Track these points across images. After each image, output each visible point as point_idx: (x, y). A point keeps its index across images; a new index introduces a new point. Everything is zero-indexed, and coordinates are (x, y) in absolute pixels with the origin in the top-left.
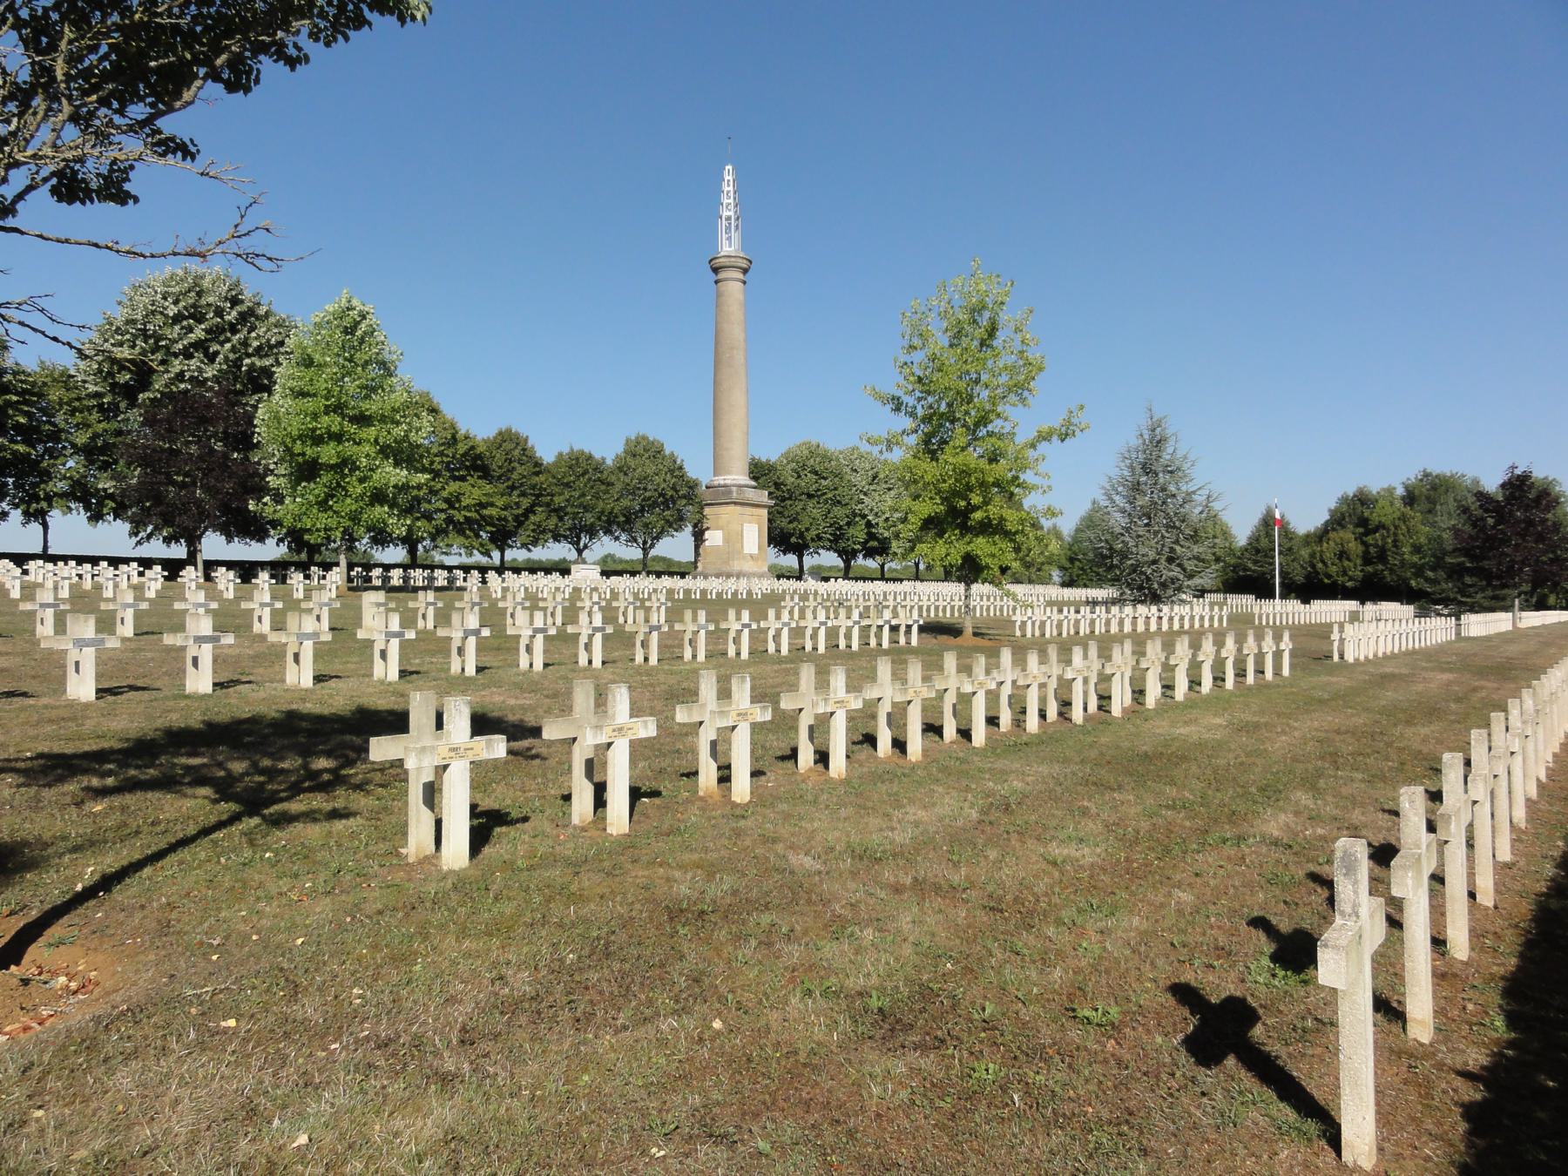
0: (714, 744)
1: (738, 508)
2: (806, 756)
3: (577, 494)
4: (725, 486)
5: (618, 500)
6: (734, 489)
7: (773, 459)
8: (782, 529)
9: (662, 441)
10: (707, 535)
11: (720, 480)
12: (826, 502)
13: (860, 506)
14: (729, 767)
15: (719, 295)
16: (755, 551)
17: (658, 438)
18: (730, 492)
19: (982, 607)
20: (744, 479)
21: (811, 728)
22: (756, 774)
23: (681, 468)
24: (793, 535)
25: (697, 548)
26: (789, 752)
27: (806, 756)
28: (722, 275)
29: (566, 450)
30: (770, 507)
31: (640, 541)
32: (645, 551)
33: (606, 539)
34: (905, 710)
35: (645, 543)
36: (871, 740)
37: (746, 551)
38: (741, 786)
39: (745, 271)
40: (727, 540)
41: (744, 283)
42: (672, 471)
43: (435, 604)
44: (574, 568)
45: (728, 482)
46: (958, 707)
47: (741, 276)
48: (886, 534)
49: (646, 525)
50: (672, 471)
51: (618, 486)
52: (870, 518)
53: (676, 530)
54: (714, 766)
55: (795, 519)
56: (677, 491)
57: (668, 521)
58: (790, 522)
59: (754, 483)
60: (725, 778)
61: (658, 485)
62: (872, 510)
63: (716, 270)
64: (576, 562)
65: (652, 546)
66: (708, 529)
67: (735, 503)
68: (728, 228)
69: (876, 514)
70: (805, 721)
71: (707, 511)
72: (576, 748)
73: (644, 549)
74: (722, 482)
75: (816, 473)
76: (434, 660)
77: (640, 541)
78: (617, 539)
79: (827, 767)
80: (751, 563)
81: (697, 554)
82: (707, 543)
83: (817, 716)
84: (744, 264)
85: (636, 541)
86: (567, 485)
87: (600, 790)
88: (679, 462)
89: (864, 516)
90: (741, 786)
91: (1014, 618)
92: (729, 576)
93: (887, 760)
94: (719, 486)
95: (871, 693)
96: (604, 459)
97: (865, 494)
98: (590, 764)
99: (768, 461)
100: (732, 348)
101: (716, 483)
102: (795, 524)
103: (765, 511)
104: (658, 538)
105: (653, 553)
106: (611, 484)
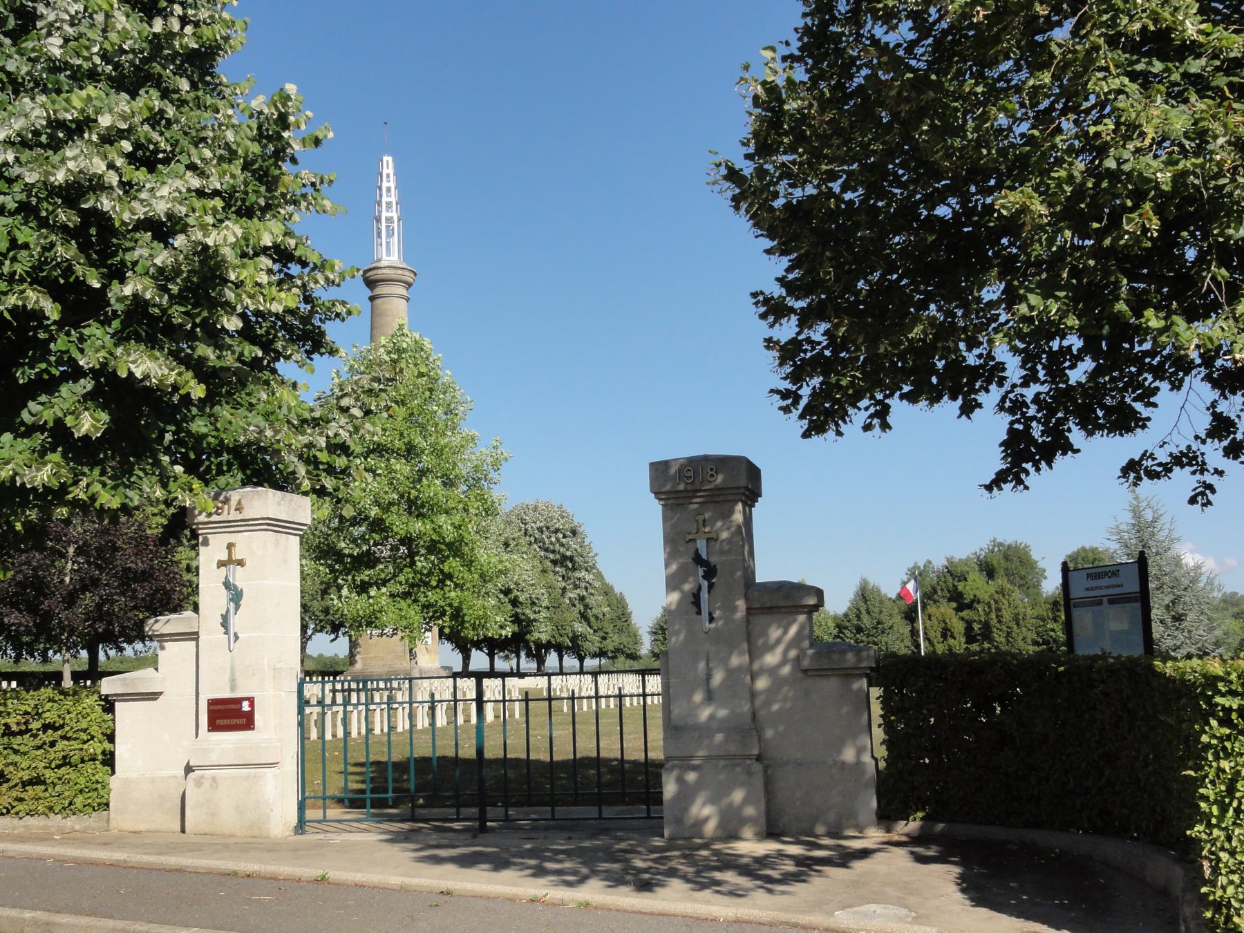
41: (408, 300)
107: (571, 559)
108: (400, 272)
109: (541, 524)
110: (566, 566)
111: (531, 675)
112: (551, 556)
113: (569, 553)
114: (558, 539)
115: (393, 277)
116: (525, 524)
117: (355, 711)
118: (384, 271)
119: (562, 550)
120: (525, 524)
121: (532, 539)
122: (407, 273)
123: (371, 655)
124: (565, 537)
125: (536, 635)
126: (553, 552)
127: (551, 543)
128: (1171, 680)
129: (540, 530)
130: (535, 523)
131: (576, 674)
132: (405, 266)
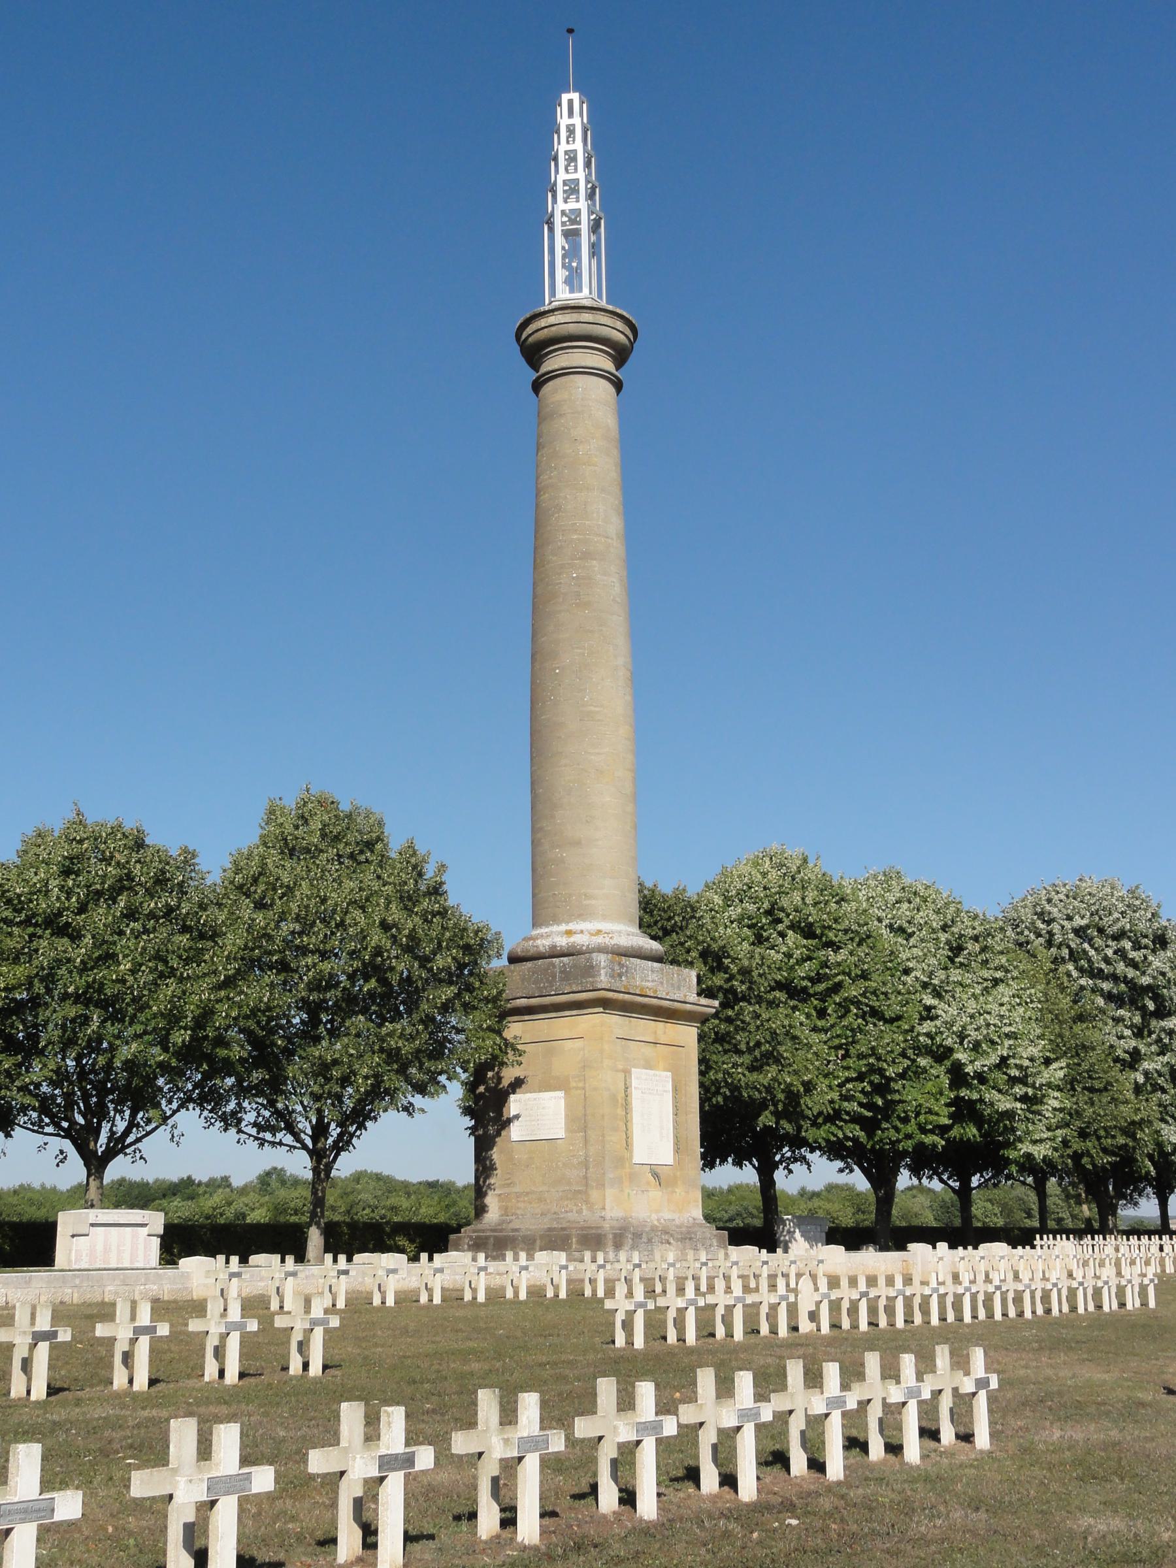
0: (495, 1481)
1: (614, 1022)
2: (608, 1498)
3: (79, 954)
4: (570, 953)
5: (229, 983)
6: (602, 959)
7: (692, 892)
8: (735, 1088)
9: (377, 810)
10: (515, 1104)
11: (553, 936)
12: (844, 1008)
13: (927, 1026)
14: (513, 1509)
15: (542, 416)
16: (664, 1154)
17: (364, 802)
18: (590, 970)
19: (942, 1298)
20: (629, 935)
21: (614, 1463)
22: (546, 1514)
23: (436, 891)
24: (763, 1106)
25: (483, 1146)
26: (587, 1489)
27: (608, 1498)
28: (552, 363)
29: (57, 822)
30: (704, 1020)
31: (304, 1126)
32: (322, 1159)
33: (190, 1119)
34: (733, 1439)
35: (320, 1131)
36: (693, 1475)
37: (640, 1155)
38: (529, 1528)
39: (621, 355)
40: (579, 1121)
41: (618, 385)
42: (408, 901)
43: (54, 1335)
44: (67, 1222)
45: (581, 940)
46: (808, 1435)
47: (608, 365)
48: (1005, 1104)
49: (323, 1069)
50: (408, 901)
51: (233, 941)
52: (961, 1056)
53: (421, 1089)
54: (496, 1508)
55: (772, 1057)
56: (424, 961)
57: (392, 1055)
58: (755, 1067)
59: (655, 946)
60: (509, 1521)
61: (363, 936)
62: (962, 1036)
63: (534, 353)
64: (78, 1198)
65: (343, 1143)
66: (517, 1084)
67: (606, 1004)
68: (573, 252)
69: (976, 1046)
70: (607, 1453)
71: (515, 1029)
72: (344, 1484)
73: (317, 1155)
74: (562, 942)
75: (808, 931)
76: (118, 1412)
77: (304, 1126)
78: (231, 1121)
79: (634, 1506)
80: (656, 1194)
81: (484, 1167)
82: (516, 1132)
83: (621, 1447)
84: (617, 332)
85: (291, 1128)
86: (56, 925)
87: (369, 1533)
88: (430, 871)
89: (941, 1054)
90: (529, 1528)
91: (609, 1304)
92: (593, 1240)
93: (714, 1498)
94: (555, 953)
95: (688, 1414)
96: (189, 856)
97: (937, 994)
98: (358, 1504)
99: (679, 893)
100: (587, 556)
101: (543, 944)
102: (772, 1071)
103: (688, 1034)
104: (360, 1116)
105: (345, 1166)
106: (211, 935)
107: (1152, 991)
108: (587, 317)
109: (1084, 922)
110: (1143, 1008)
111: (930, 1236)
112: (1106, 986)
113: (1145, 980)
114: (1121, 952)
115: (573, 329)
116: (1049, 923)
117: (1081, 1288)
118: (552, 319)
119: (1131, 973)
120: (1049, 923)
121: (1065, 952)
122: (619, 325)
123: (517, 1189)
124: (1137, 946)
125: (1025, 1148)
126: (1115, 978)
127: (1107, 960)
128: (224, 1224)
129: (1079, 932)
130: (1069, 918)
131: (1150, 1233)
132: (610, 308)
